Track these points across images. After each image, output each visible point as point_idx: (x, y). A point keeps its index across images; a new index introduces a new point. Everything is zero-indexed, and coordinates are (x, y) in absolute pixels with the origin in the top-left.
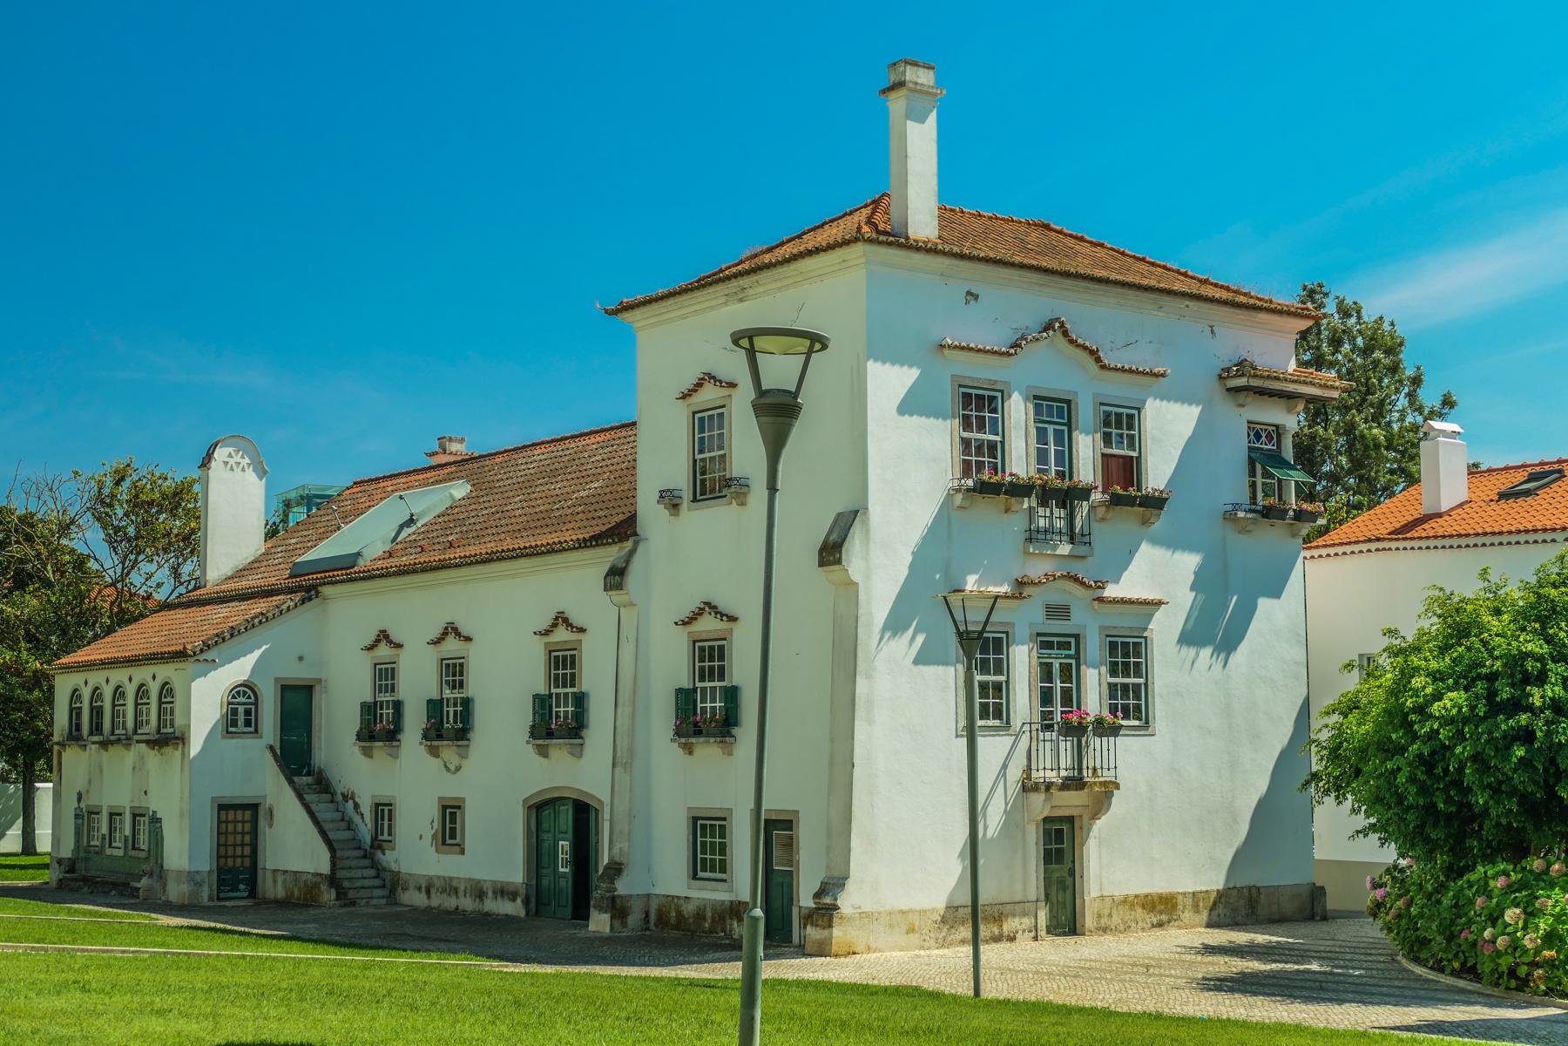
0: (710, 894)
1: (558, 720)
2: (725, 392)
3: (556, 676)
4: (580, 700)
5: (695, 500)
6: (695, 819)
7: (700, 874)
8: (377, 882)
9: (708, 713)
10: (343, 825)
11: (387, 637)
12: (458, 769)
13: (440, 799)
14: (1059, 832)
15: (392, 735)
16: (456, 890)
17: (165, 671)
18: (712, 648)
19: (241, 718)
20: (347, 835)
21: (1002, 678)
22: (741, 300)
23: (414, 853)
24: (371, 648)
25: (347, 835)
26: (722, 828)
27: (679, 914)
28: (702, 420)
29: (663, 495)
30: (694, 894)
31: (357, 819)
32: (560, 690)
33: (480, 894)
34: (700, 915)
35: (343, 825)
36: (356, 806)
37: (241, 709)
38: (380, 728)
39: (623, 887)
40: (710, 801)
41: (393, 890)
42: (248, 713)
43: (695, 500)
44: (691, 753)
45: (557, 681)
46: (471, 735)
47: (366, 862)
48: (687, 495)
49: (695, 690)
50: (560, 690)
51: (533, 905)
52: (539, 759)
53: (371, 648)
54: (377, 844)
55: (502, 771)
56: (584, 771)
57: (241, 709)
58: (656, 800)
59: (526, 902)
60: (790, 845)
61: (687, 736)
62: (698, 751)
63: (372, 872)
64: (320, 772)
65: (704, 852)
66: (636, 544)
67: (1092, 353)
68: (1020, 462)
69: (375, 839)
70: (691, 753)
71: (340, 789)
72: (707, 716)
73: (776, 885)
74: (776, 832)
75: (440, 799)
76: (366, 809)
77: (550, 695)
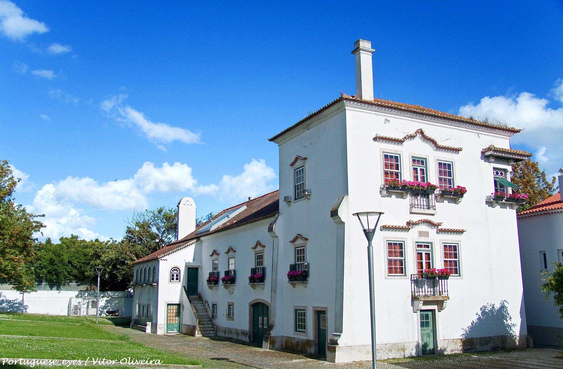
0: (301, 337)
1: (257, 277)
2: (303, 161)
3: (298, 257)
4: (264, 269)
5: (295, 199)
6: (296, 310)
7: (298, 329)
8: (212, 329)
9: (299, 275)
10: (205, 311)
11: (260, 244)
12: (233, 293)
13: (228, 303)
14: (427, 316)
15: (216, 282)
16: (232, 332)
17: (150, 264)
18: (301, 250)
19: (175, 277)
20: (205, 314)
21: (403, 258)
22: (308, 129)
23: (222, 321)
24: (255, 248)
25: (205, 314)
26: (304, 313)
27: (292, 343)
28: (297, 172)
29: (285, 198)
30: (296, 336)
31: (208, 309)
32: (300, 263)
33: (238, 334)
34: (297, 344)
35: (205, 311)
36: (208, 305)
37: (175, 275)
38: (213, 280)
39: (273, 333)
40: (300, 304)
41: (216, 332)
42: (177, 275)
43: (295, 199)
44: (294, 287)
45: (299, 259)
46: (309, 279)
47: (210, 322)
48: (293, 198)
49: (256, 268)
50: (300, 263)
51: (252, 338)
52: (252, 289)
53: (255, 248)
54: (214, 317)
55: (244, 294)
56: (263, 294)
57: (175, 275)
58: (285, 304)
59: (250, 337)
60: (325, 320)
61: (292, 281)
62: (297, 286)
63: (211, 326)
64: (200, 295)
65: (299, 322)
66: (278, 216)
67: (178, 206)
68: (407, 176)
69: (212, 315)
70: (294, 287)
71: (204, 300)
72: (299, 275)
73: (321, 333)
74: (320, 314)
75: (228, 303)
76: (211, 306)
77: (296, 264)
